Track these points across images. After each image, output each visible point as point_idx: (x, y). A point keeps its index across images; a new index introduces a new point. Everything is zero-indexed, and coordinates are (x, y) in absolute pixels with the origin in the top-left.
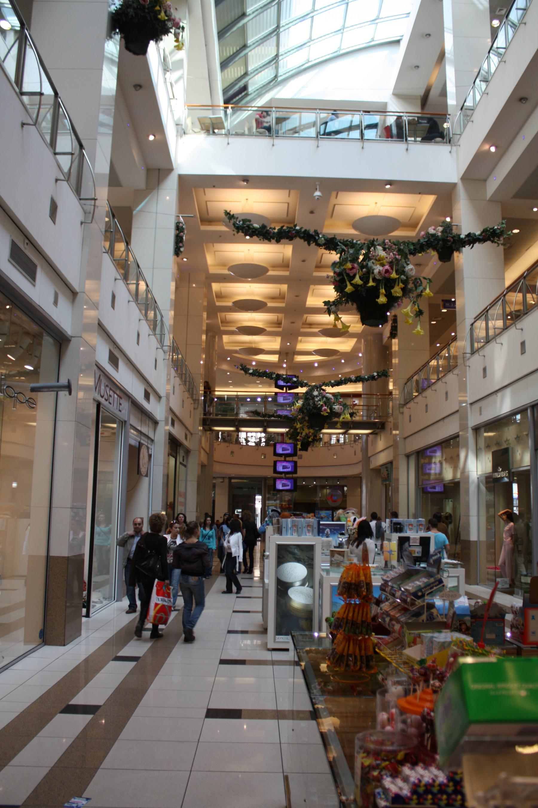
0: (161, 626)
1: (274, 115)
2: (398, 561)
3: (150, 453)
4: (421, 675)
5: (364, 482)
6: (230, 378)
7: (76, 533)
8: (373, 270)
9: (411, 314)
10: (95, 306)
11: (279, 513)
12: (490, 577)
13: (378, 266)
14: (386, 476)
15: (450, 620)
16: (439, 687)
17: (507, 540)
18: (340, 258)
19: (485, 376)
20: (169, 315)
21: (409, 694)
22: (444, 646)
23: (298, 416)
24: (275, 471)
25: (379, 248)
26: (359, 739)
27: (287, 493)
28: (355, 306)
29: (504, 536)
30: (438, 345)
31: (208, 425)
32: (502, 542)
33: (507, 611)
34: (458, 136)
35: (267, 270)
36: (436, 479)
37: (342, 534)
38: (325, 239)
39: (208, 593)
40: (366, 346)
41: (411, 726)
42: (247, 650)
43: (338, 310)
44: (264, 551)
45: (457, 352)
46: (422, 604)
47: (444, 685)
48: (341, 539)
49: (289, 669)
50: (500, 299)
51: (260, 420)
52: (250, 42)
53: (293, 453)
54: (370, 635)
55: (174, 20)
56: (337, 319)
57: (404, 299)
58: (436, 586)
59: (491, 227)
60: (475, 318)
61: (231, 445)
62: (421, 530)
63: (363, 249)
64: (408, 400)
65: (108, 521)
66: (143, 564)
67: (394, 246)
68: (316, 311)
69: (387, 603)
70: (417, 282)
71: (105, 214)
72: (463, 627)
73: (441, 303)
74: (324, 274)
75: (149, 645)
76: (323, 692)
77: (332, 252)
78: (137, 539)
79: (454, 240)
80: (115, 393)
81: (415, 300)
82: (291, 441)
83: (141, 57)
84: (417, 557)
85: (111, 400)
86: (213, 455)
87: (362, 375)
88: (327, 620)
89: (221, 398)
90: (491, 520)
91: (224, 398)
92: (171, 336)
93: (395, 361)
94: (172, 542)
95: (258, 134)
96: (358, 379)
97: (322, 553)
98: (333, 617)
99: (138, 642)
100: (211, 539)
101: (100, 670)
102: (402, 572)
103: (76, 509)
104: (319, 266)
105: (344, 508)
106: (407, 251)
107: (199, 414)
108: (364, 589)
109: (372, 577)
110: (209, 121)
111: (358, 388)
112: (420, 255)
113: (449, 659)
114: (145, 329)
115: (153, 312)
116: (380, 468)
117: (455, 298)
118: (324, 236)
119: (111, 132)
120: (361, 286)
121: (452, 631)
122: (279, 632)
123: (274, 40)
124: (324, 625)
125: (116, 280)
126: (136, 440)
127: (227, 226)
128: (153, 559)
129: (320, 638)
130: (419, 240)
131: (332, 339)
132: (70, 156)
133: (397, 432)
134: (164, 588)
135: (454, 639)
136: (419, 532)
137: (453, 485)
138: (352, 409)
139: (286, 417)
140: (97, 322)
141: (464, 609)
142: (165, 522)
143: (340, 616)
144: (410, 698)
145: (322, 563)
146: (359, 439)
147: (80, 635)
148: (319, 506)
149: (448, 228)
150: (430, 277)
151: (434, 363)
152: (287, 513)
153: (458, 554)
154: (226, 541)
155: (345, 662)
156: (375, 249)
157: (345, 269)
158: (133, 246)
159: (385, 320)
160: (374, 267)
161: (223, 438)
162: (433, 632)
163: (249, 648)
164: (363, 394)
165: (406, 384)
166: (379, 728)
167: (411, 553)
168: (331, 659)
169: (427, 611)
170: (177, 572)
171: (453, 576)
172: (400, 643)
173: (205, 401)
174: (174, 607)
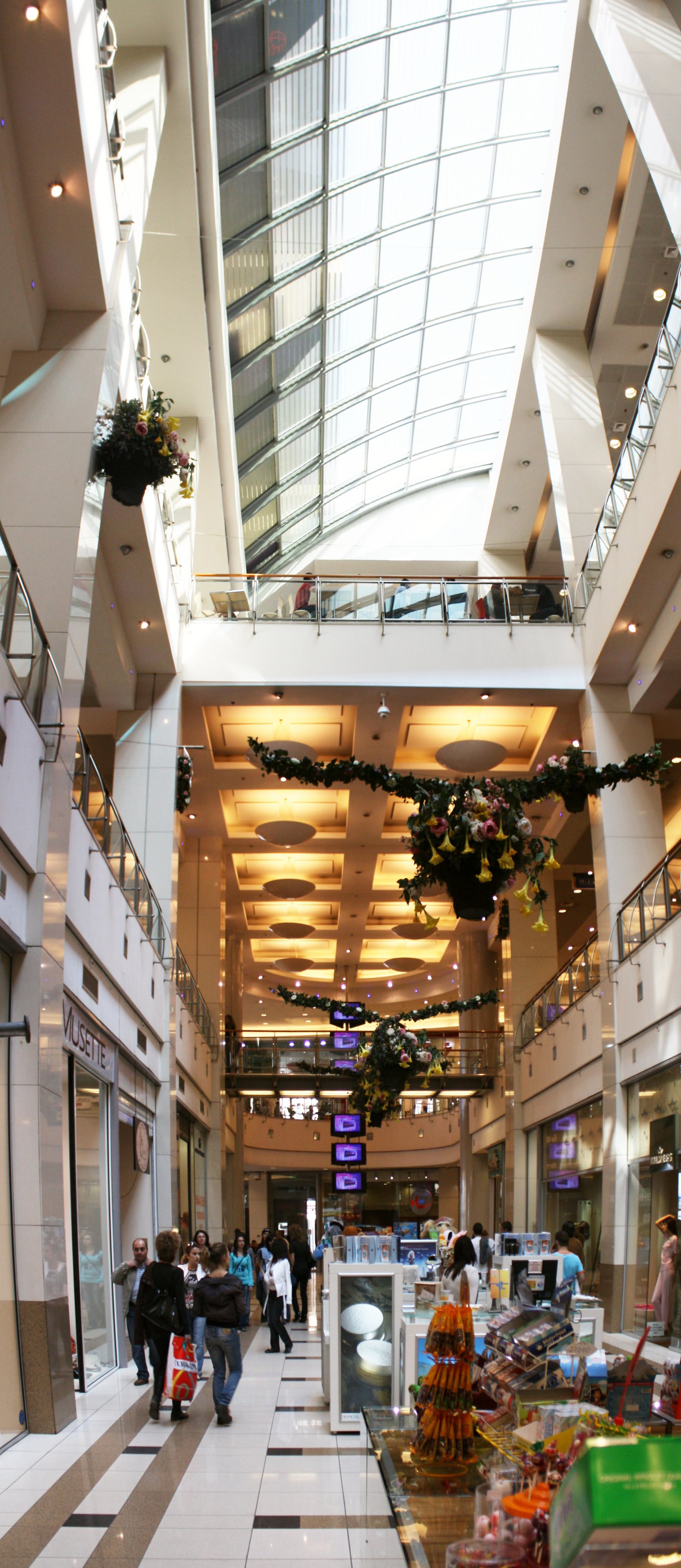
0: (184, 1403)
1: (319, 588)
2: (511, 1298)
3: (151, 1134)
4: (536, 1464)
5: (463, 1175)
6: (263, 1009)
7: (53, 1265)
8: (470, 827)
9: (528, 898)
10: (61, 895)
11: (342, 1228)
12: (638, 1320)
13: (477, 821)
14: (496, 1165)
15: (579, 1386)
16: (557, 1481)
17: (666, 1263)
18: (420, 809)
19: (640, 998)
20: (170, 908)
21: (518, 1491)
22: (568, 1423)
23: (365, 1070)
24: (334, 1161)
25: (477, 791)
26: (451, 1552)
27: (353, 1196)
28: (445, 887)
29: (662, 1256)
30: (570, 948)
31: (234, 1087)
32: (658, 1266)
33: (658, 1371)
34: (582, 610)
35: (313, 831)
36: (568, 1169)
37: (433, 1259)
38: (397, 780)
39: (245, 1353)
40: (464, 952)
41: (519, 1533)
42: (303, 1434)
43: (420, 894)
44: (322, 1288)
45: (598, 959)
46: (542, 1363)
47: (565, 1477)
48: (430, 1267)
49: (359, 1460)
50: (660, 870)
51: (311, 1078)
52: (282, 479)
53: (359, 1130)
54: (469, 1410)
55: (180, 456)
56: (420, 908)
57: (519, 876)
58: (562, 1335)
59: (639, 754)
60: (624, 903)
61: (269, 1120)
62: (544, 1250)
63: (453, 794)
64: (527, 1041)
65: (97, 1246)
66: (152, 1310)
67: (499, 789)
68: (386, 896)
69: (494, 1363)
70: (536, 845)
71: (74, 746)
72: (597, 1395)
73: (573, 879)
74: (397, 836)
75: (170, 1430)
76: (406, 1490)
77: (407, 799)
78: (140, 1273)
79: (586, 777)
80: (94, 1037)
81: (534, 874)
82: (355, 1111)
83: (133, 508)
84: (538, 1292)
85: (89, 1049)
86: (242, 1136)
87: (459, 1001)
88: (411, 1389)
89: (251, 1043)
90: (645, 1231)
91: (256, 1042)
92: (175, 942)
93: (507, 976)
94: (191, 1275)
95: (296, 617)
96: (453, 1006)
97: (404, 1289)
98: (419, 1384)
99: (155, 1427)
100: (246, 1271)
101: (108, 1467)
102: (515, 1316)
103: (50, 1227)
104: (390, 823)
105: (435, 1218)
106: (518, 796)
107: (219, 1070)
108: (462, 1343)
109: (475, 1323)
110: (225, 598)
111: (452, 1021)
112: (538, 801)
113: (573, 1441)
114: (135, 931)
115: (146, 903)
116: (486, 1152)
117: (592, 870)
118: (395, 774)
119: (88, 615)
120: (453, 852)
121: (581, 1401)
122: (346, 1408)
123: (314, 432)
124: (408, 1396)
125: (90, 851)
126: (128, 1114)
127: (252, 761)
128: (165, 1303)
129: (402, 1416)
130: (535, 778)
131: (412, 943)
132: (29, 660)
133: (512, 1093)
134: (184, 1346)
135: (583, 1413)
136: (542, 1253)
137: (591, 1177)
138: (445, 1056)
139: (348, 1071)
140: (64, 922)
141: (599, 1368)
142: (179, 1245)
143: (429, 1383)
144: (519, 1496)
145: (403, 1301)
146: (456, 1105)
147: (75, 1418)
148: (399, 1215)
149: (576, 756)
150: (554, 837)
151: (564, 977)
152: (352, 1227)
153: (596, 1286)
154: (268, 1272)
155: (435, 1449)
156: (471, 794)
157: (428, 827)
158: (116, 797)
159: (489, 909)
160: (472, 823)
161: (256, 1108)
162: (555, 1404)
163: (306, 1432)
164: (461, 1032)
165: (523, 1013)
166: (477, 1536)
167: (529, 1287)
168: (417, 1445)
169: (548, 1373)
170: (201, 1322)
171: (587, 1320)
172: (509, 1421)
173: (227, 1047)
174: (201, 1375)
